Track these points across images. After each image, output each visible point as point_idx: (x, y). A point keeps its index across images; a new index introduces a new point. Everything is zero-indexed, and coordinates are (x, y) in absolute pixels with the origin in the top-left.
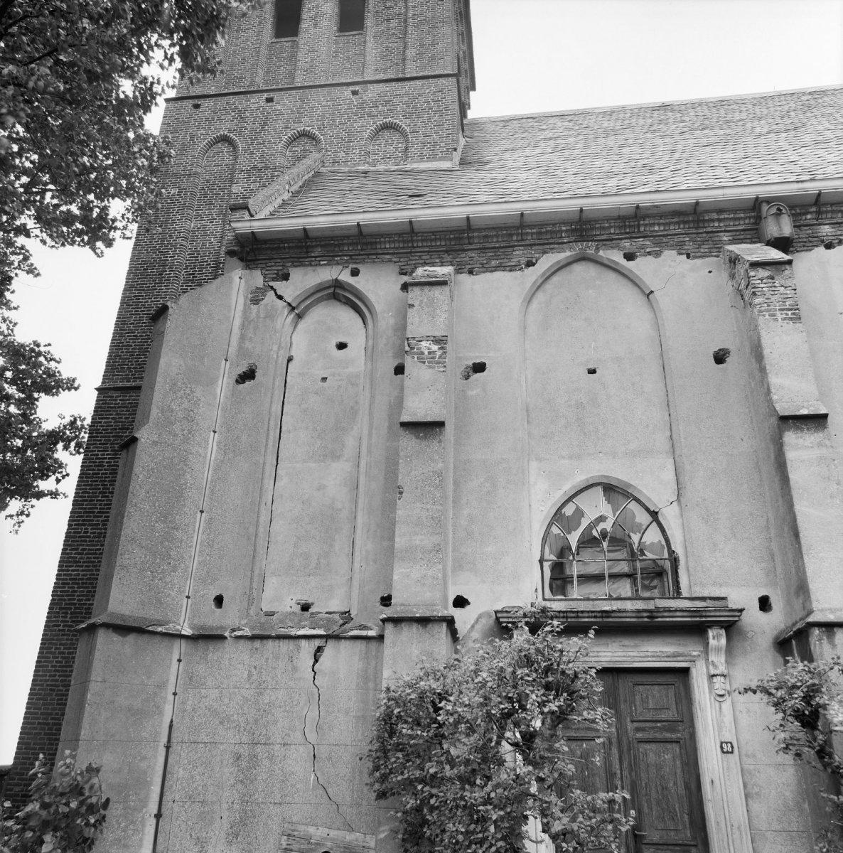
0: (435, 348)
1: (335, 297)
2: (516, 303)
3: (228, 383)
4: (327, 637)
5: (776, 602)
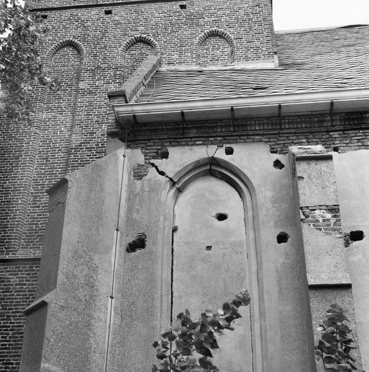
0: (329, 216)
1: (211, 173)
3: (120, 252)
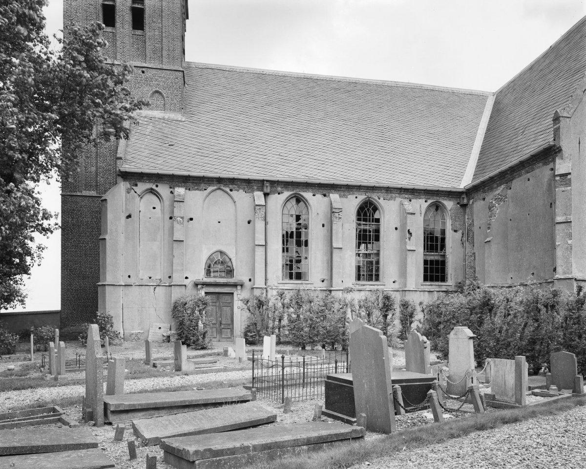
1: (151, 192)
4: (157, 286)
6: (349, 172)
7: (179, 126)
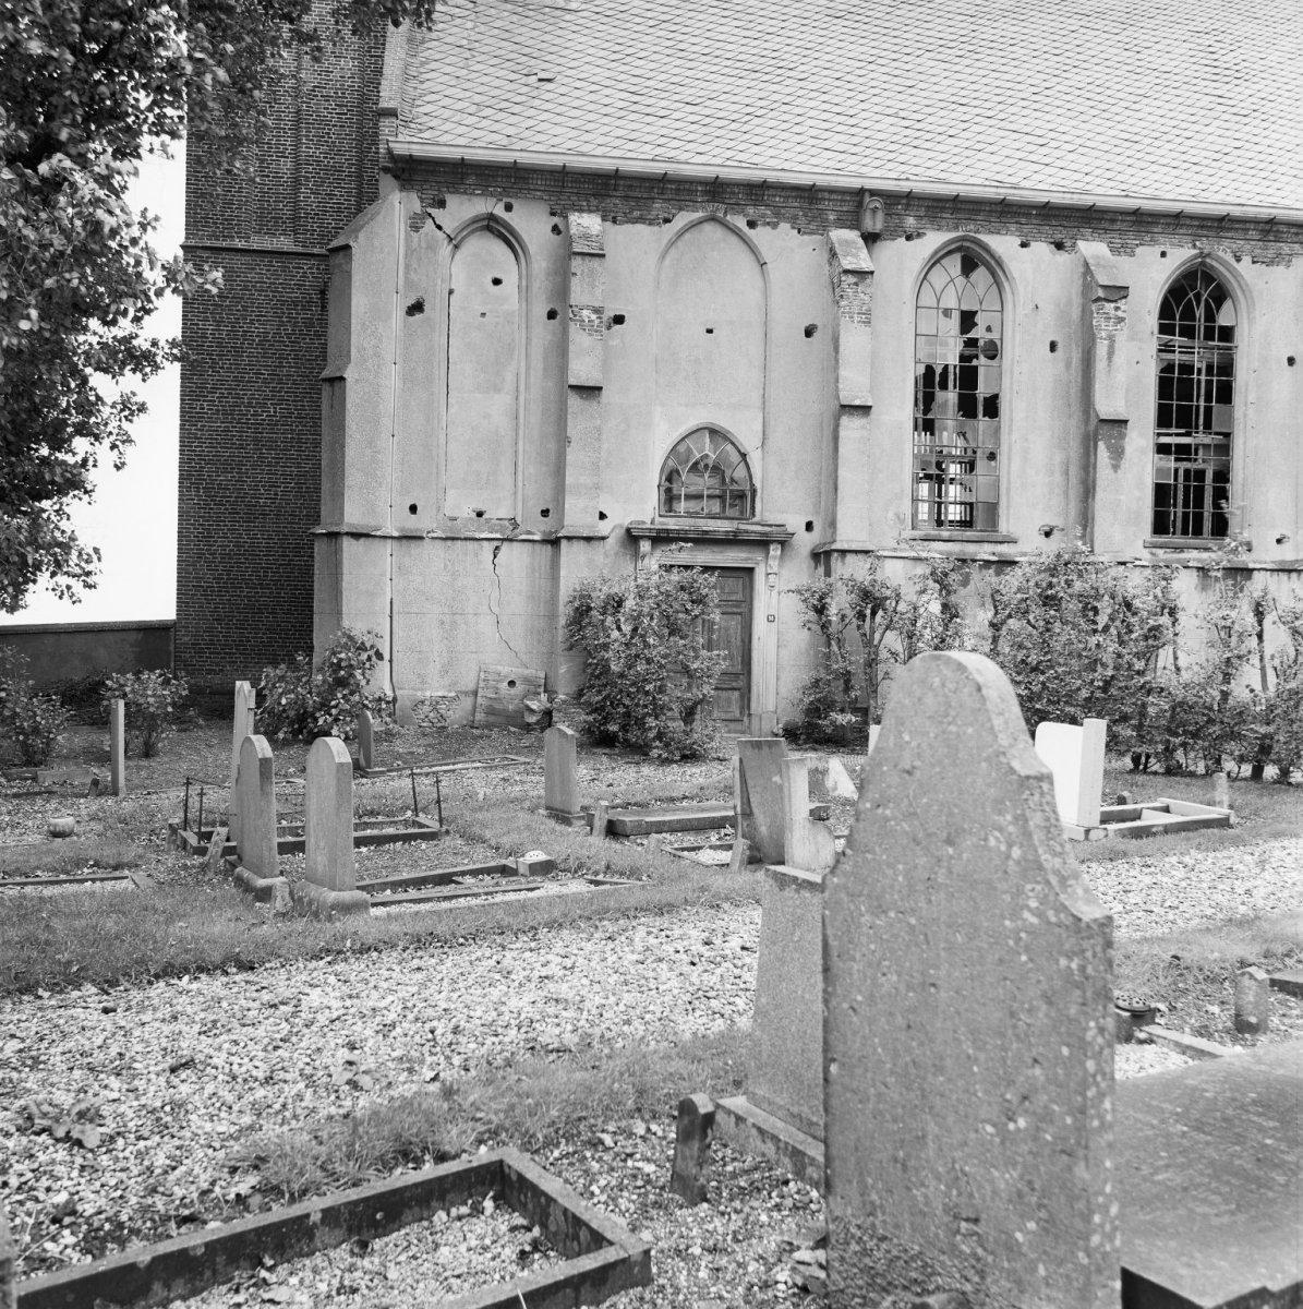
0: (594, 317)
1: (489, 228)
2: (653, 259)
4: (503, 540)
5: (817, 526)
6: (1130, 171)
7: (563, 25)
